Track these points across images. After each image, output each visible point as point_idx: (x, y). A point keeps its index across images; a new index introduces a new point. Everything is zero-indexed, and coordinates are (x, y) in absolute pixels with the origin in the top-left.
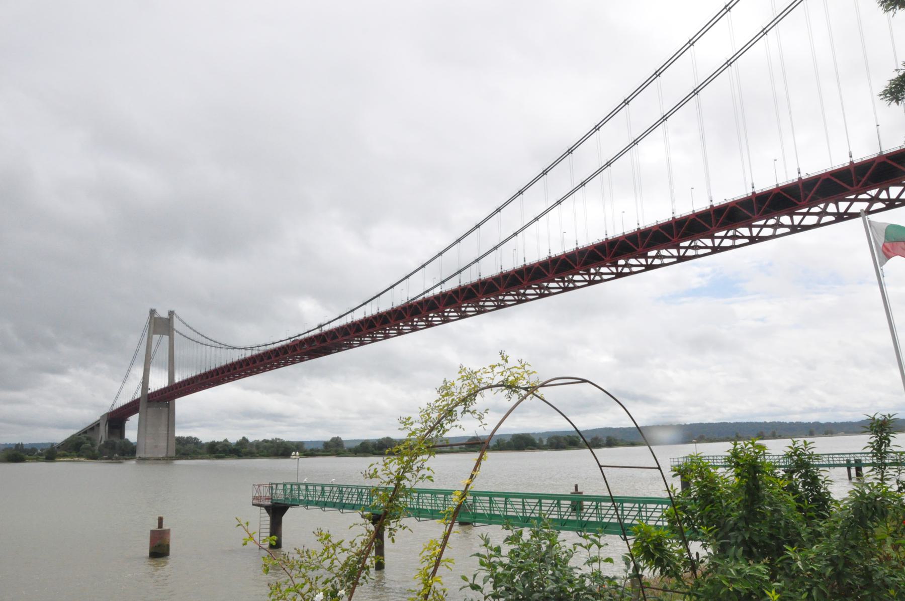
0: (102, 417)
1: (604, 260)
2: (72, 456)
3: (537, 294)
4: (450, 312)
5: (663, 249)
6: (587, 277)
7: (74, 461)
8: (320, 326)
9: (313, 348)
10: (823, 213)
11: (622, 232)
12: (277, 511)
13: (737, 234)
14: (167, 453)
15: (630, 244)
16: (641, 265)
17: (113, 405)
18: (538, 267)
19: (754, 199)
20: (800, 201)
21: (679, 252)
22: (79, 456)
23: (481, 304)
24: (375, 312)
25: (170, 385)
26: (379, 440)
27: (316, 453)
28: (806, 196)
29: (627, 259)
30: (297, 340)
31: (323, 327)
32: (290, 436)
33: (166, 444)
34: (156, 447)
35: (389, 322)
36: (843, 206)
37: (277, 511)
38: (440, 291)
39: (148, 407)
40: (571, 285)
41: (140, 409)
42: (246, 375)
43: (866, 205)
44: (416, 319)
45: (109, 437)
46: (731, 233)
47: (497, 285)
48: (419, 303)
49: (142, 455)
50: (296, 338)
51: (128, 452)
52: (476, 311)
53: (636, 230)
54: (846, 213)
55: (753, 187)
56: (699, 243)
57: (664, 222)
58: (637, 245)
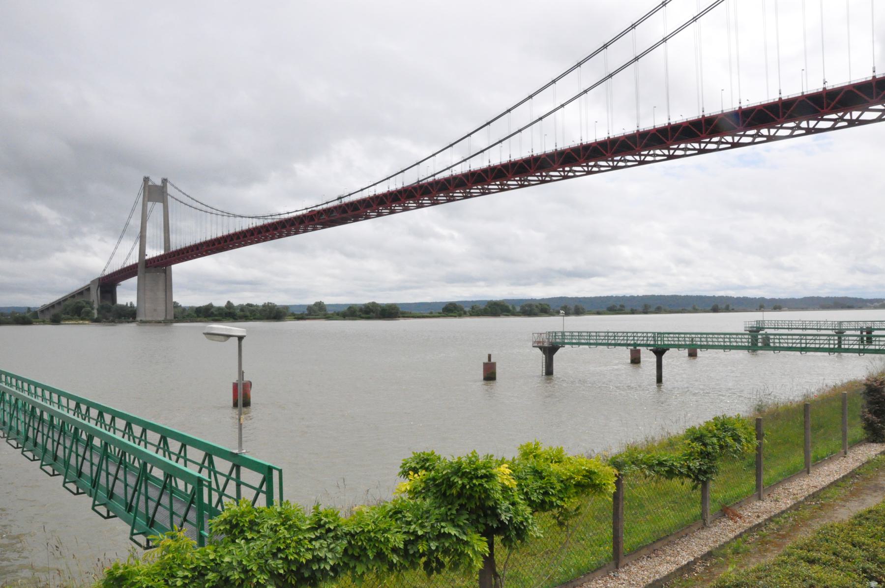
0: (93, 282)
1: (699, 136)
2: (75, 319)
3: (539, 180)
4: (396, 206)
5: (658, 149)
6: (586, 169)
7: (79, 324)
8: (340, 198)
9: (333, 218)
10: (758, 135)
11: (721, 110)
12: (550, 350)
13: (723, 140)
14: (166, 316)
15: (863, 96)
16: (664, 155)
17: (105, 270)
18: (544, 158)
19: (703, 122)
20: (779, 118)
21: (669, 152)
22: (82, 319)
23: (420, 202)
24: (399, 186)
25: (167, 252)
26: (365, 305)
27: (307, 317)
28: (828, 105)
29: (596, 161)
30: (314, 210)
31: (343, 199)
32: (280, 300)
33: (164, 308)
34: (155, 310)
35: (385, 203)
36: (773, 131)
37: (550, 350)
38: (450, 173)
39: (145, 272)
40: (526, 183)
41: (139, 273)
42: (198, 256)
43: (832, 123)
44: (381, 208)
45: (101, 302)
46: (652, 152)
47: (506, 172)
48: (430, 184)
49: (144, 319)
50: (313, 209)
51: (128, 315)
52: (447, 200)
53: (635, 132)
54: (857, 119)
55: (780, 94)
56: (689, 146)
57: (694, 119)
58: (579, 156)
